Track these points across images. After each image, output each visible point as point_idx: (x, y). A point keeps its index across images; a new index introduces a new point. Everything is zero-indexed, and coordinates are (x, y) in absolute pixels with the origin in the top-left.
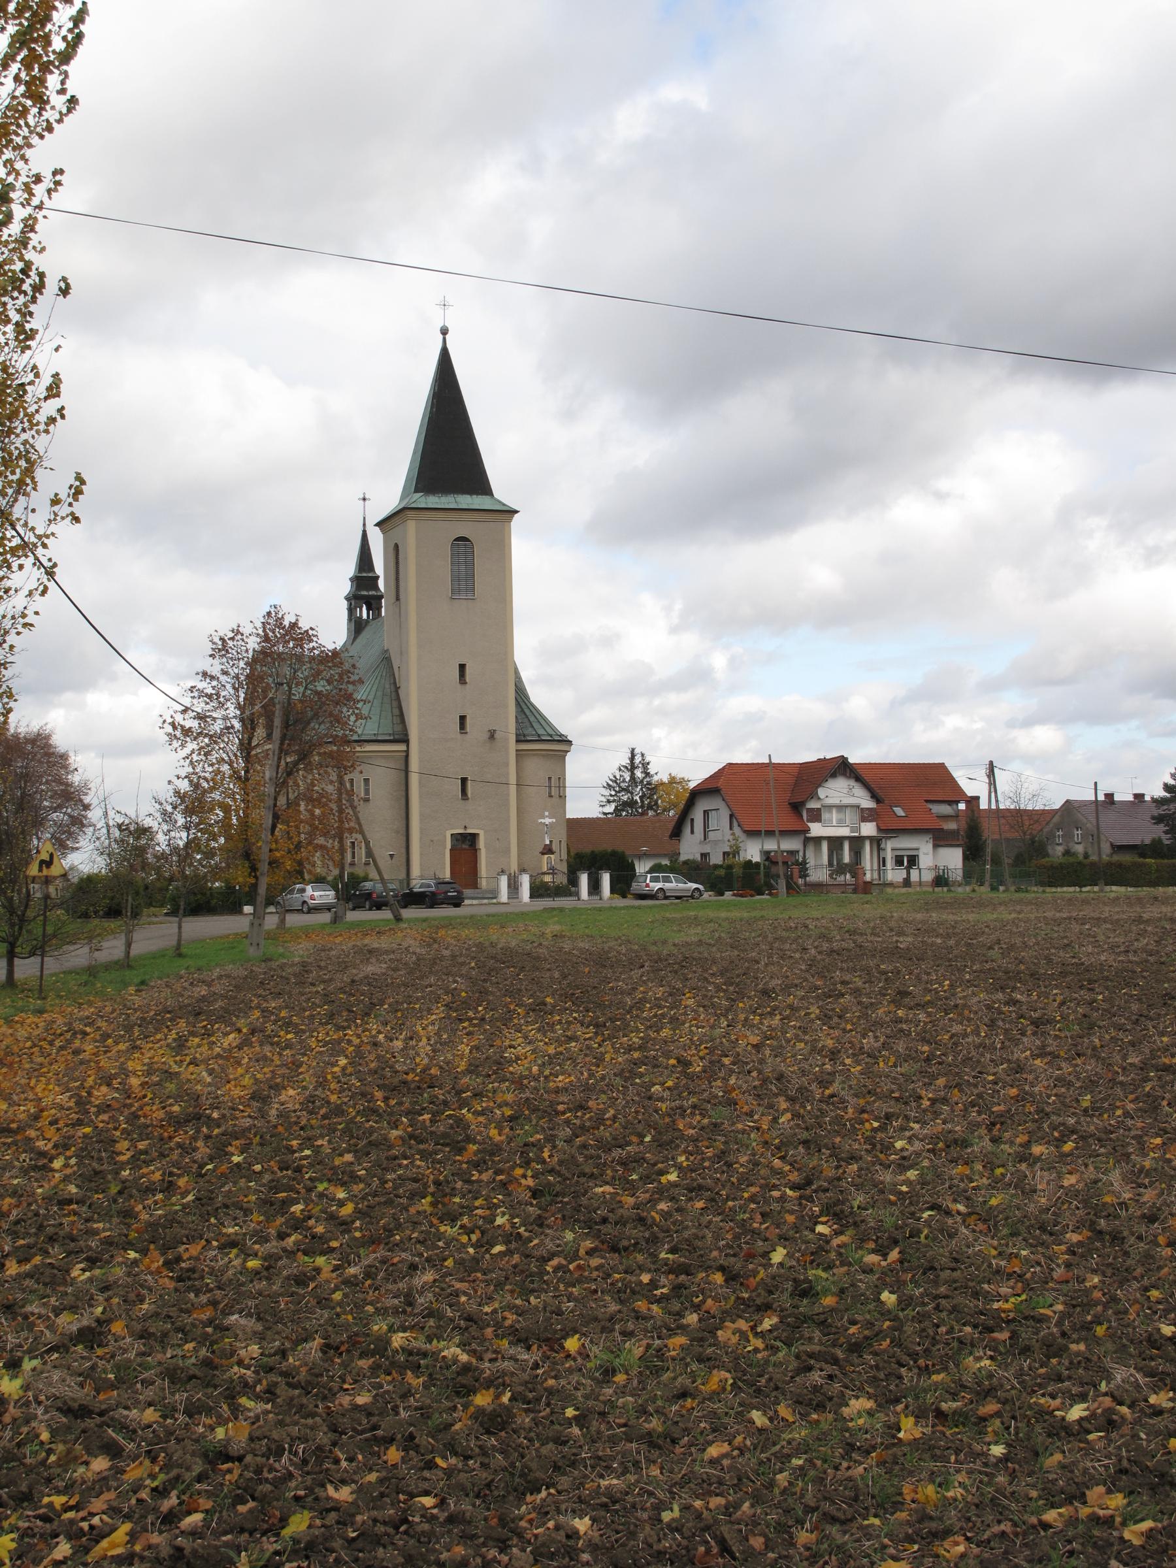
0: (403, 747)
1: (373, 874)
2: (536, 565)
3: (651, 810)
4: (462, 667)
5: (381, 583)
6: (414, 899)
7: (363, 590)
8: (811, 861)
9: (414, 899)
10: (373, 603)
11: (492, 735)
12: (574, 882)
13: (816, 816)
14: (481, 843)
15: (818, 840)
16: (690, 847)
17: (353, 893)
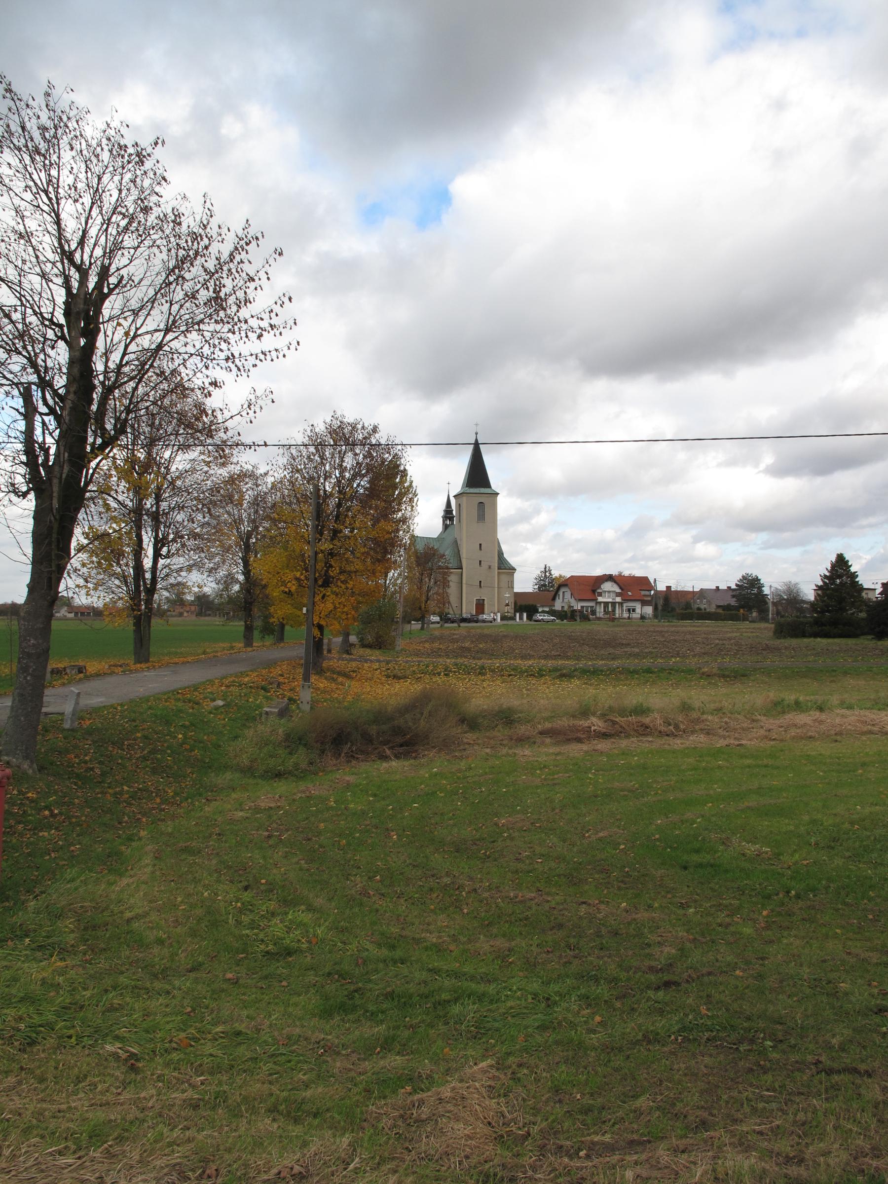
1: (451, 612)
2: (506, 506)
3: (551, 587)
5: (454, 513)
6: (464, 620)
7: (448, 514)
8: (598, 610)
9: (464, 620)
10: (451, 519)
11: (490, 567)
12: (515, 615)
13: (600, 595)
14: (486, 602)
15: (600, 603)
16: (558, 605)
17: (445, 619)
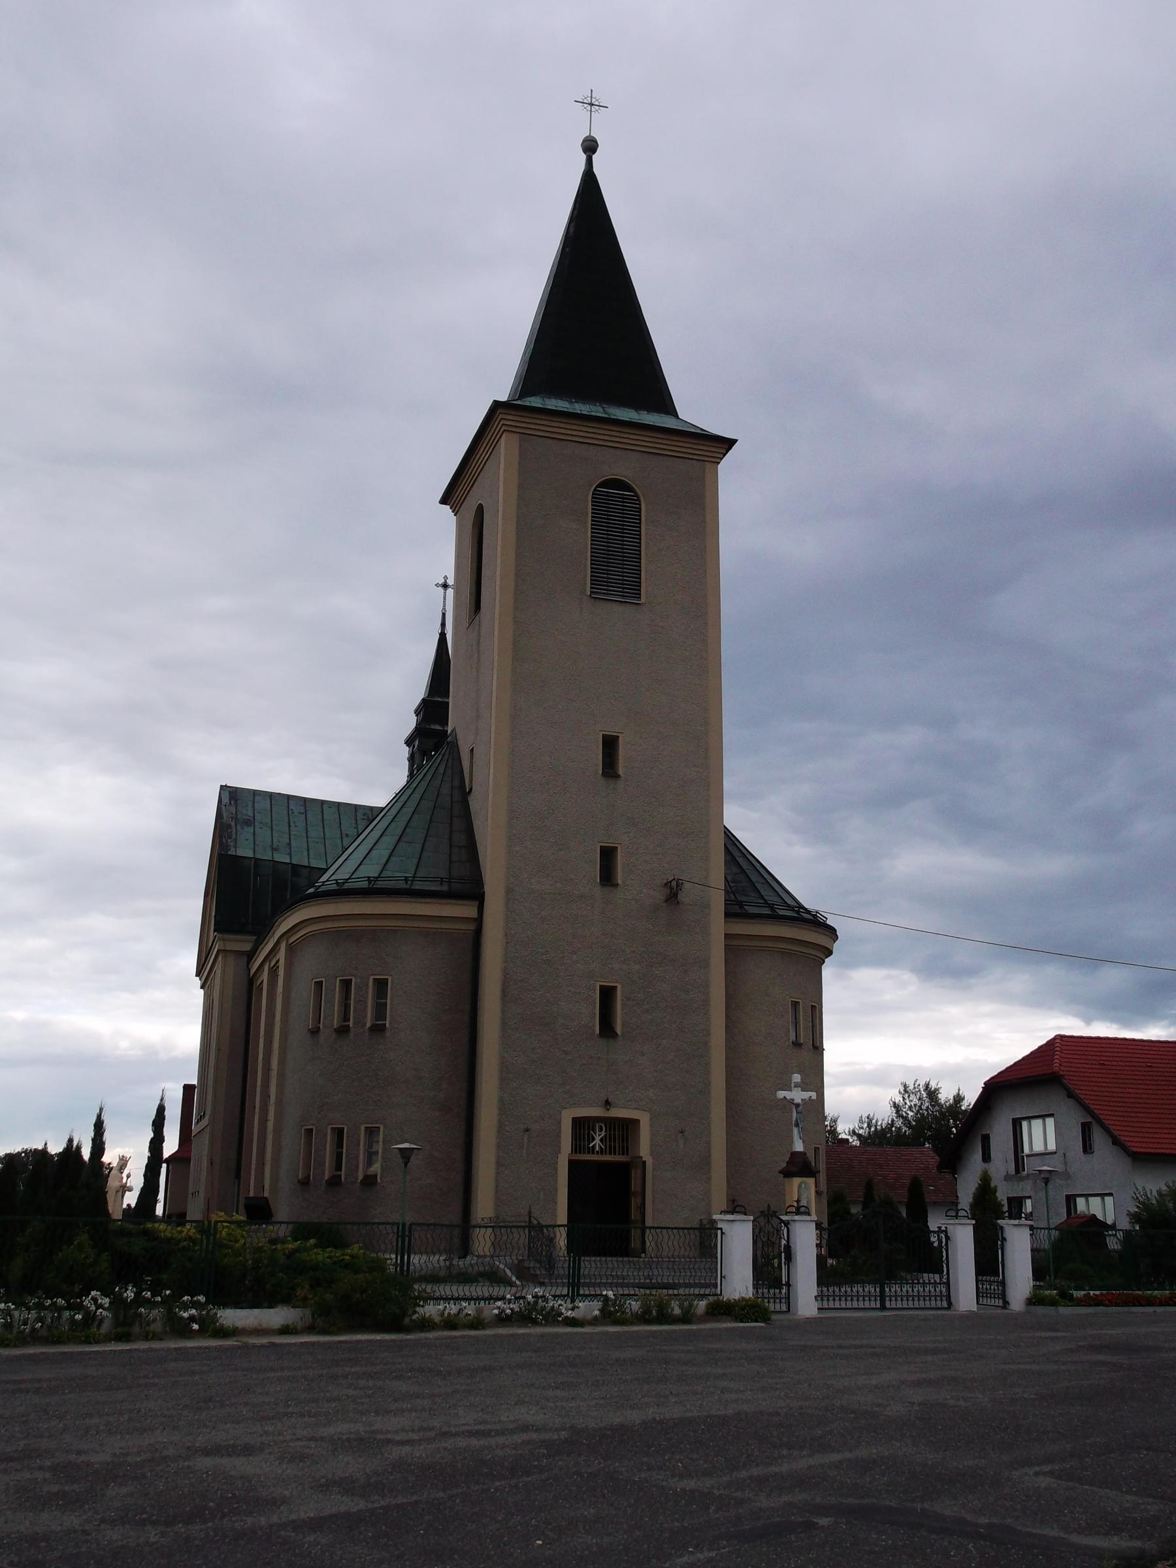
0: (467, 910)
4: (610, 744)
11: (673, 893)
